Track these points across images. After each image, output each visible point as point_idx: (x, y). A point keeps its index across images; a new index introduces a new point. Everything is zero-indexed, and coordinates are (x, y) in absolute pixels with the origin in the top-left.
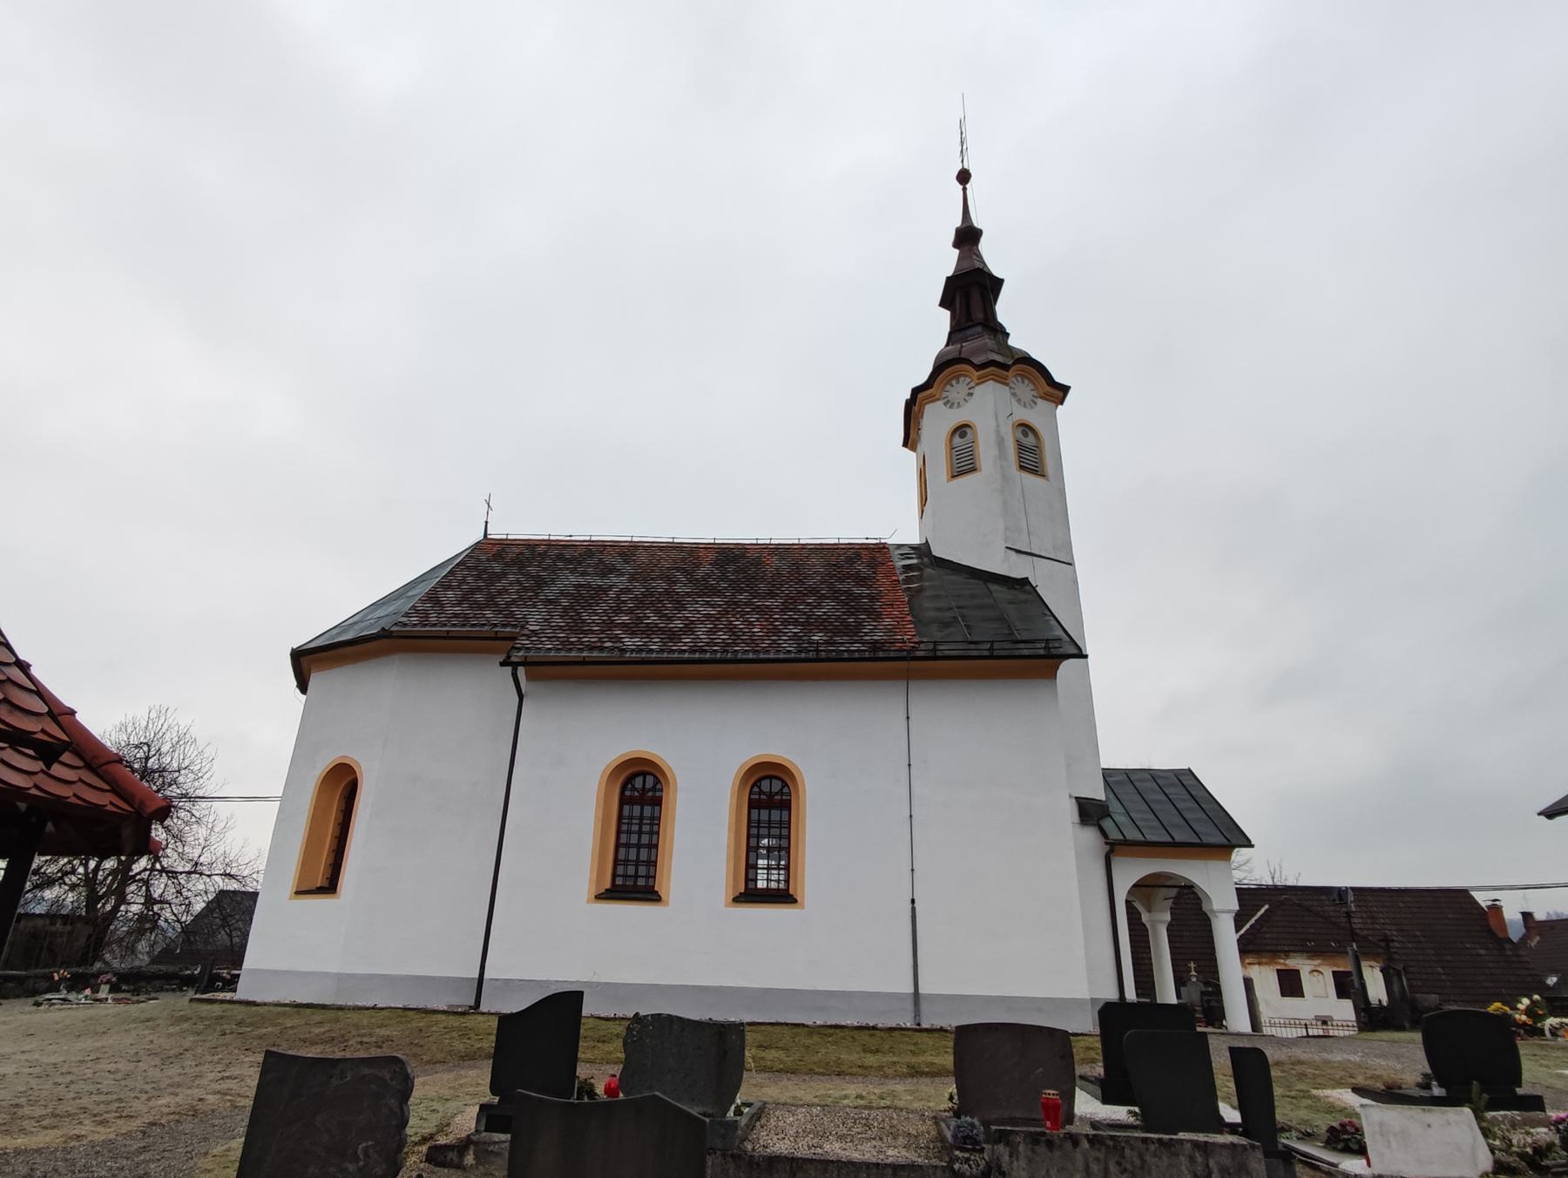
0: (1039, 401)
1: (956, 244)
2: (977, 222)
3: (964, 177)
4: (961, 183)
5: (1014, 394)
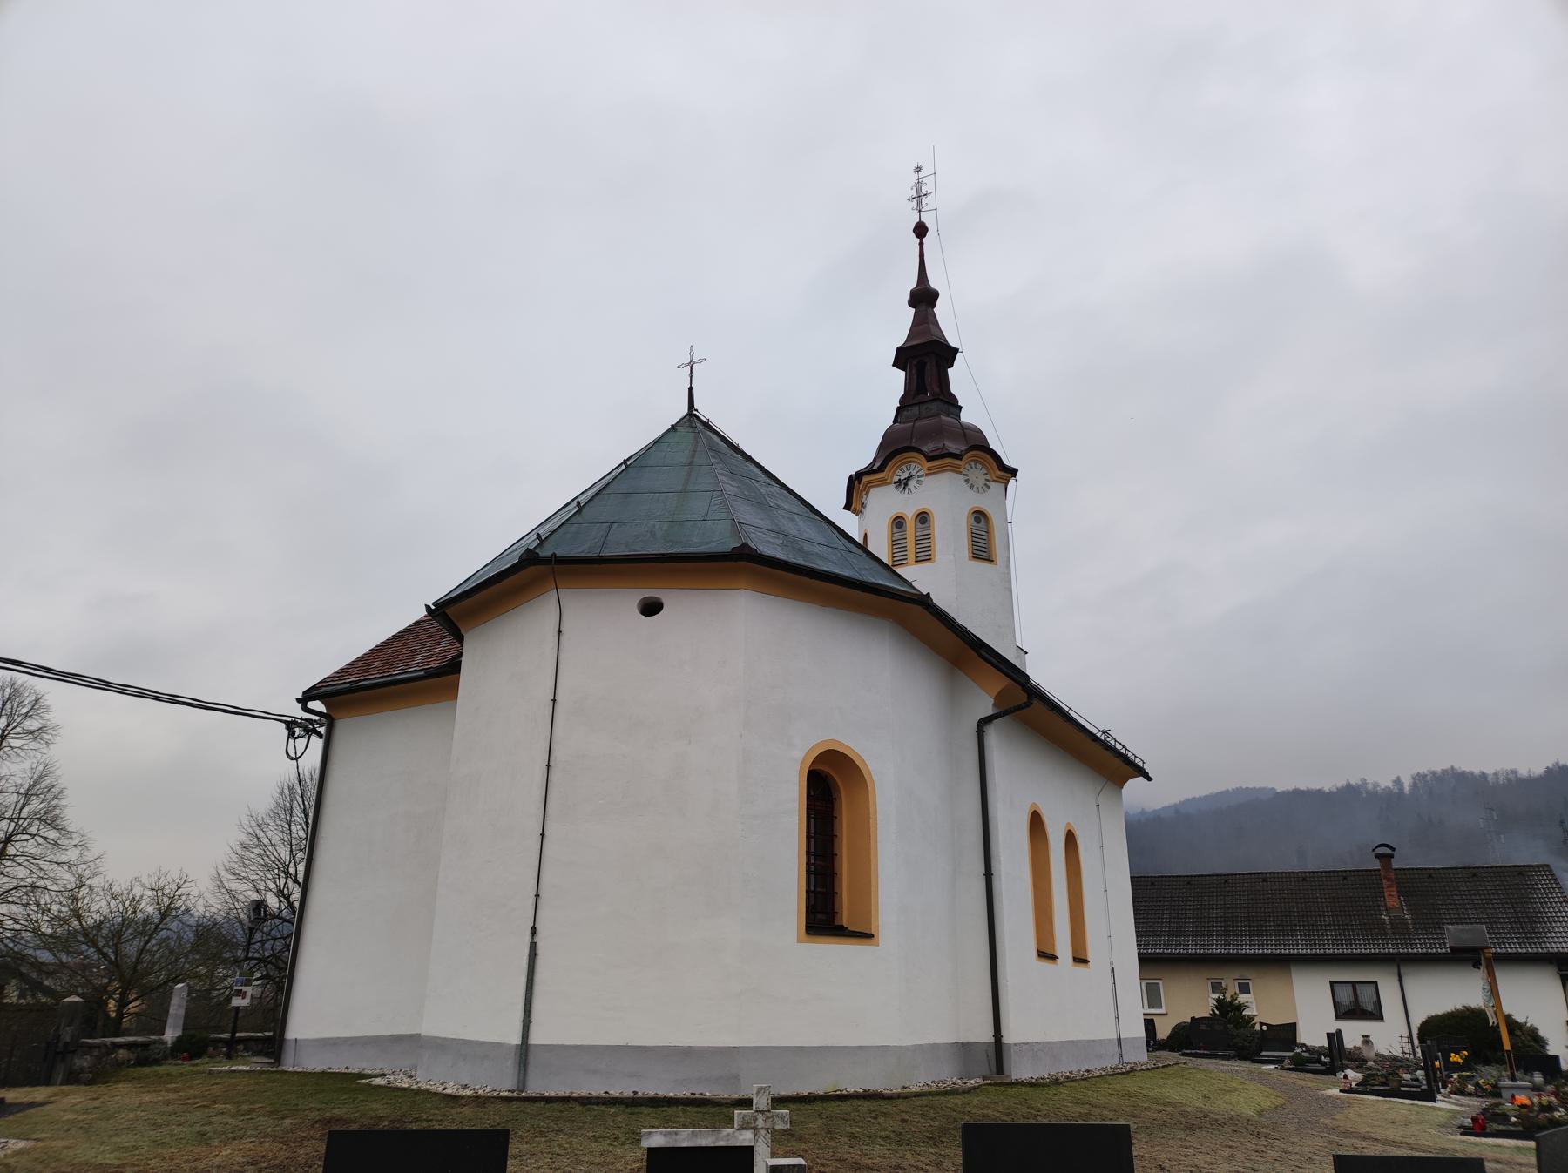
0: (992, 485)
1: (912, 303)
2: (934, 282)
3: (921, 230)
4: (917, 236)
5: (967, 481)
